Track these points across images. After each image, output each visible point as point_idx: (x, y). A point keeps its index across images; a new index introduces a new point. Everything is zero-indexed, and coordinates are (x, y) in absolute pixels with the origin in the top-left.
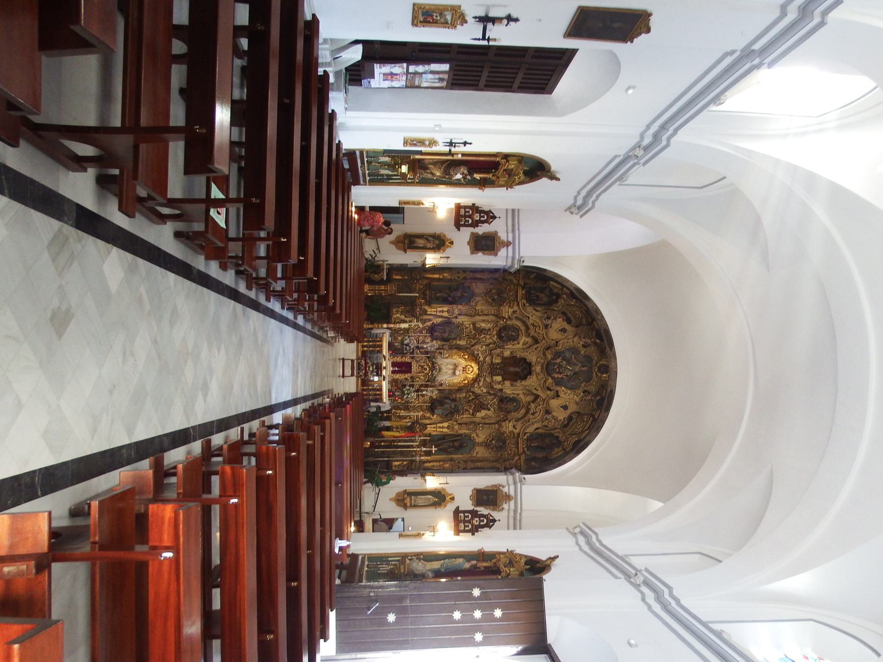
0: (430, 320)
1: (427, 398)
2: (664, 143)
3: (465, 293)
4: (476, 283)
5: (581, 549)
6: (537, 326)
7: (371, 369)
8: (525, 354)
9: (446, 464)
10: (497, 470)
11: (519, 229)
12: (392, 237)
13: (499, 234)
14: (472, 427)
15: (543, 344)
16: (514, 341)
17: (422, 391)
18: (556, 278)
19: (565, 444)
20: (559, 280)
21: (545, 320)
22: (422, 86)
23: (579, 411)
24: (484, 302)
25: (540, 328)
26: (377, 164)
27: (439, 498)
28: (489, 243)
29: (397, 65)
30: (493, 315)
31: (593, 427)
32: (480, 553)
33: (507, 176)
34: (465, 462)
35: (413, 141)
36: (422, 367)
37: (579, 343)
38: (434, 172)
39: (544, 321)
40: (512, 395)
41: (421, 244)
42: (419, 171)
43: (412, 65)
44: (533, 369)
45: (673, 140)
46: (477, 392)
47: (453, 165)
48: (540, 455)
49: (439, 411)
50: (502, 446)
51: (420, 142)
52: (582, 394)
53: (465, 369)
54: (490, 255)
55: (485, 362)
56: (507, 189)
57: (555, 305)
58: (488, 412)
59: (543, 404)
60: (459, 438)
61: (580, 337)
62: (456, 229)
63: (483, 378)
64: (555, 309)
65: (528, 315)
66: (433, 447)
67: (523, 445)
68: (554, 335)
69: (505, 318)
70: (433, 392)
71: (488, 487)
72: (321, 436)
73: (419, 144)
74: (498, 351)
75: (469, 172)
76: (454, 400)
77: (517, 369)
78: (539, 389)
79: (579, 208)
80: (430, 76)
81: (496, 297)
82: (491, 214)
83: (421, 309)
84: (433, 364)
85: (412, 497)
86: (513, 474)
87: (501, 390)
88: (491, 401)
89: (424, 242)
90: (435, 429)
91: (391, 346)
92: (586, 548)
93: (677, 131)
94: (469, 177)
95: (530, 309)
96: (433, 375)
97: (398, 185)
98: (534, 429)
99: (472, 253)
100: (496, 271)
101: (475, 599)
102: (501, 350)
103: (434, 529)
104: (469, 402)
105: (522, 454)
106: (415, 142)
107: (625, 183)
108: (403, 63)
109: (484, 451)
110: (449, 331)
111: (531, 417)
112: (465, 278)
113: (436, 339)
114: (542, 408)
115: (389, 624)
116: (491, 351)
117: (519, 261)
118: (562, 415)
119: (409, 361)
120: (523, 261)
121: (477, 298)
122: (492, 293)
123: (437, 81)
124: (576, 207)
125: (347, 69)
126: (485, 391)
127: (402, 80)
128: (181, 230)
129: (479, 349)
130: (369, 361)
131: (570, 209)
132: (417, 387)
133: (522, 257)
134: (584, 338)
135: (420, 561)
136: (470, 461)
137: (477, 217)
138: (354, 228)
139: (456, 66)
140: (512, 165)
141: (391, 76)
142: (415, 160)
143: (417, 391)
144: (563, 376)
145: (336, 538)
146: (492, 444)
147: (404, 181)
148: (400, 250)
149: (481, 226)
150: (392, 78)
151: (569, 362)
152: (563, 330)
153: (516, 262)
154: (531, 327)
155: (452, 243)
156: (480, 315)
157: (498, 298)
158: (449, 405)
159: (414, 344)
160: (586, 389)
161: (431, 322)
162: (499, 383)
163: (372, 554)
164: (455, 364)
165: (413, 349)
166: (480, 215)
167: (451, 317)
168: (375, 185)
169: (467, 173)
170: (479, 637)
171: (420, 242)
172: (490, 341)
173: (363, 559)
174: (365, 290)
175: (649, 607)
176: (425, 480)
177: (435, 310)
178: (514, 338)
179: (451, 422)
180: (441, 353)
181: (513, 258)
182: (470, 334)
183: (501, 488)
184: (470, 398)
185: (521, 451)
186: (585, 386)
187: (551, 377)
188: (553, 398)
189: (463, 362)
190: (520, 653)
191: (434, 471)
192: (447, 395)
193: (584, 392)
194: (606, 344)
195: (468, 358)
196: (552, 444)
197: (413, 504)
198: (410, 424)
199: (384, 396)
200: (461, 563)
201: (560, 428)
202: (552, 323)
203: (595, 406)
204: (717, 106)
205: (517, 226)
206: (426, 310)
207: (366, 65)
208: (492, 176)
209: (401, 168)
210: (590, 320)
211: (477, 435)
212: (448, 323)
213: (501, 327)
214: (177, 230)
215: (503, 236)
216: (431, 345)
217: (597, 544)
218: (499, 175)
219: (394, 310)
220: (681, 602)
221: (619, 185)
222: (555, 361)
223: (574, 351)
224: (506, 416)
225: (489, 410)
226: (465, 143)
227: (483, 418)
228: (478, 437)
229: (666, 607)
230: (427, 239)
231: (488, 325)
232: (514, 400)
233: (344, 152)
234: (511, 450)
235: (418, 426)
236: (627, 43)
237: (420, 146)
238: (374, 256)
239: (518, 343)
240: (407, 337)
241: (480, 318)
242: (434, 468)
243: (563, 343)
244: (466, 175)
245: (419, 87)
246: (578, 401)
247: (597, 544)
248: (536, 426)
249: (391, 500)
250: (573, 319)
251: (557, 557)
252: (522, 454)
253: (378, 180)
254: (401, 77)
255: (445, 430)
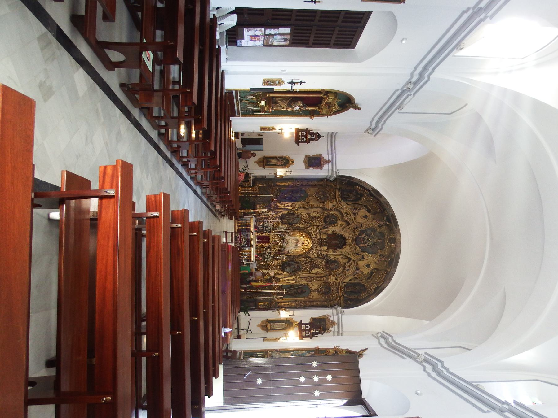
0: (281, 212)
1: (280, 261)
2: (426, 78)
3: (303, 194)
4: (309, 188)
5: (382, 346)
6: (349, 214)
7: (244, 240)
8: (342, 232)
9: (293, 303)
10: (326, 307)
11: (335, 153)
12: (255, 159)
13: (323, 156)
14: (309, 279)
15: (353, 226)
16: (334, 224)
17: (277, 256)
18: (359, 183)
19: (369, 289)
20: (362, 184)
21: (354, 210)
22: (274, 44)
23: (378, 268)
24: (314, 200)
25: (350, 215)
26: (246, 101)
27: (289, 323)
28: (317, 161)
29: (258, 29)
30: (320, 208)
31: (387, 278)
32: (316, 349)
33: (327, 107)
34: (305, 302)
35: (269, 81)
36: (276, 241)
37: (376, 225)
38: (281, 105)
39: (353, 211)
40: (334, 259)
41: (275, 162)
42: (272, 105)
43: (267, 29)
44: (347, 241)
45: (431, 77)
46: (311, 257)
47: (294, 101)
48: (353, 297)
49: (287, 270)
50: (328, 292)
51: (273, 82)
52: (379, 257)
53: (303, 243)
54: (318, 169)
55: (316, 238)
56: (328, 117)
57: (360, 201)
58: (319, 270)
59: (354, 264)
60: (301, 286)
61: (376, 221)
62: (296, 144)
63: (315, 248)
64: (360, 203)
65: (342, 207)
66: (284, 290)
67: (342, 290)
68: (360, 220)
69: (328, 210)
70: (283, 257)
71: (320, 316)
72: (212, 245)
73: (272, 84)
74: (324, 230)
75: (303, 105)
76: (297, 263)
77: (337, 242)
78: (351, 254)
79: (374, 130)
80: (279, 37)
81: (322, 197)
82: (318, 135)
83: (274, 205)
84: (283, 239)
85: (272, 324)
86: (336, 308)
87: (327, 255)
88: (321, 263)
89: (276, 161)
90: (285, 281)
91: (256, 227)
92: (386, 346)
93: (434, 70)
94: (303, 108)
95: (344, 204)
96: (283, 246)
97: (259, 116)
98: (349, 280)
99: (306, 168)
100: (321, 180)
101: (314, 368)
102: (326, 230)
103: (286, 335)
104: (307, 263)
105: (341, 296)
106: (270, 82)
107: (401, 111)
108: (262, 28)
109: (318, 295)
110: (293, 219)
111: (347, 272)
112: (302, 185)
113: (285, 224)
114: (354, 266)
115: (258, 385)
116: (319, 230)
117: (336, 172)
118: (366, 271)
119: (268, 235)
120: (339, 172)
121: (310, 198)
122: (319, 194)
123: (283, 40)
124: (372, 129)
125: (226, 31)
126: (316, 256)
127: (261, 40)
128: (124, 82)
129: (312, 230)
130: (242, 235)
131: (368, 130)
132: (273, 254)
133: (338, 170)
134: (379, 221)
135: (277, 352)
136: (308, 302)
137: (309, 136)
138: (230, 176)
139: (295, 29)
140: (331, 99)
141: (254, 37)
142: (269, 97)
143: (273, 257)
144: (366, 246)
145: (222, 327)
146: (322, 290)
147: (263, 113)
148: (261, 167)
149: (311, 142)
150: (255, 38)
151: (370, 236)
152: (366, 217)
153: (334, 173)
154: (345, 215)
155: (293, 162)
156: (312, 208)
157: (323, 198)
158: (295, 266)
159: (270, 227)
160: (381, 253)
161: (282, 213)
162: (325, 251)
163: (246, 351)
164: (297, 240)
165: (270, 230)
166: (311, 135)
167: (294, 209)
168: (245, 116)
169: (303, 106)
170: (317, 393)
171: (274, 162)
172: (319, 224)
173: (240, 353)
174: (240, 191)
175: (429, 374)
176: (280, 313)
177: (284, 205)
178: (334, 223)
179: (296, 276)
180: (288, 233)
181: (332, 170)
182: (306, 220)
183: (329, 317)
184: (307, 261)
185: (341, 294)
186: (380, 252)
187: (359, 246)
188: (360, 260)
189: (302, 239)
190: (346, 404)
191: (285, 308)
192: (292, 259)
193: (380, 255)
194: (393, 225)
195: (305, 236)
196: (361, 290)
197: (272, 329)
198: (269, 277)
199: (253, 257)
200: (304, 353)
201: (366, 280)
202: (358, 212)
203: (387, 265)
204: (458, 50)
205: (334, 150)
206: (278, 205)
207: (239, 29)
208: (318, 109)
209: (261, 103)
210: (382, 210)
211: (312, 285)
212: (292, 213)
213: (325, 215)
214: (122, 82)
215: (325, 157)
216: (281, 227)
217: (393, 343)
218: (322, 108)
219: (258, 206)
220: (450, 370)
221: (398, 113)
222: (361, 236)
223: (373, 229)
224: (331, 272)
225: (319, 268)
226: (301, 82)
227: (315, 274)
228: (313, 286)
229: (439, 374)
230: (278, 159)
231: (318, 215)
232: (335, 262)
233: (225, 91)
234: (334, 294)
235: (274, 279)
236: (401, 3)
237: (272, 85)
238: (244, 169)
239: (337, 226)
240: (266, 222)
241: (312, 210)
242: (285, 306)
243: (366, 224)
244: (302, 107)
245: (272, 45)
246: (376, 262)
247: (393, 343)
248: (350, 278)
249: (258, 326)
250: (371, 210)
251: (367, 349)
252: (341, 296)
253: (247, 113)
254: (260, 38)
255: (292, 282)
